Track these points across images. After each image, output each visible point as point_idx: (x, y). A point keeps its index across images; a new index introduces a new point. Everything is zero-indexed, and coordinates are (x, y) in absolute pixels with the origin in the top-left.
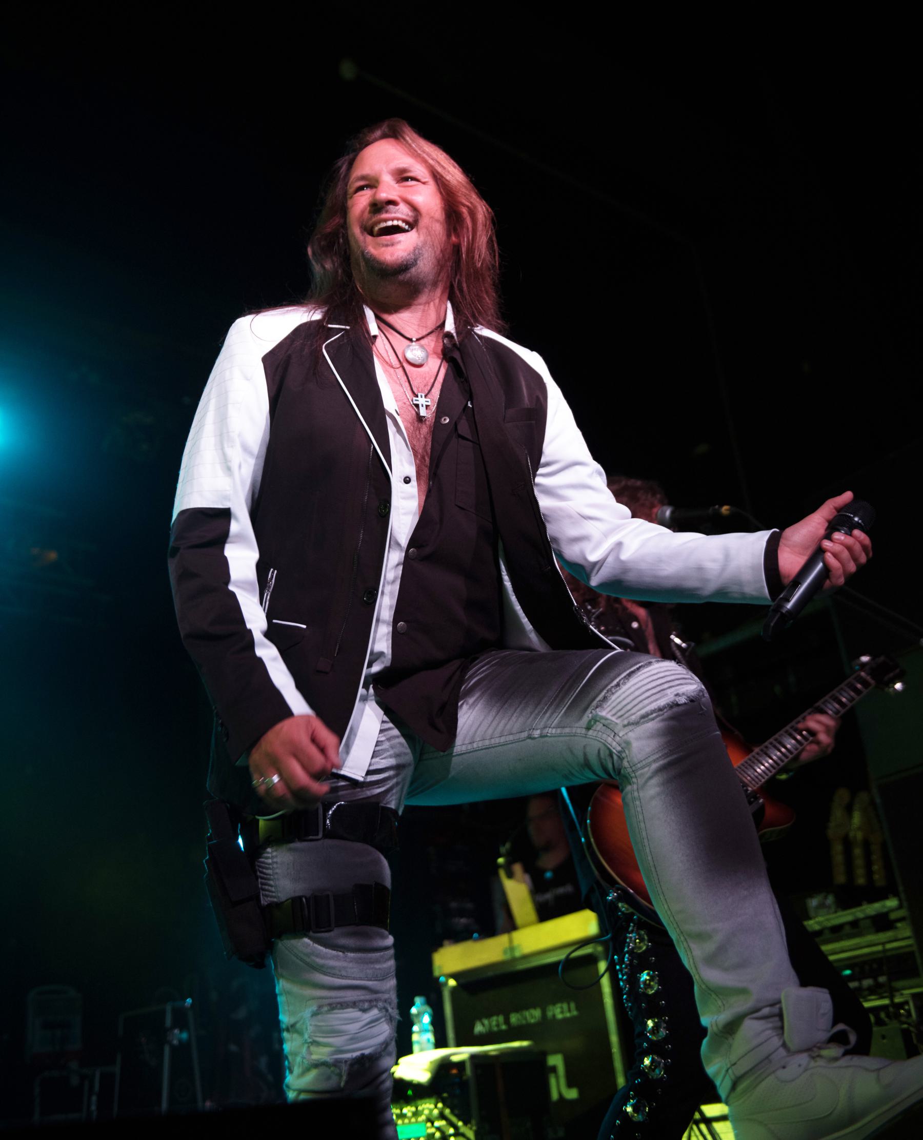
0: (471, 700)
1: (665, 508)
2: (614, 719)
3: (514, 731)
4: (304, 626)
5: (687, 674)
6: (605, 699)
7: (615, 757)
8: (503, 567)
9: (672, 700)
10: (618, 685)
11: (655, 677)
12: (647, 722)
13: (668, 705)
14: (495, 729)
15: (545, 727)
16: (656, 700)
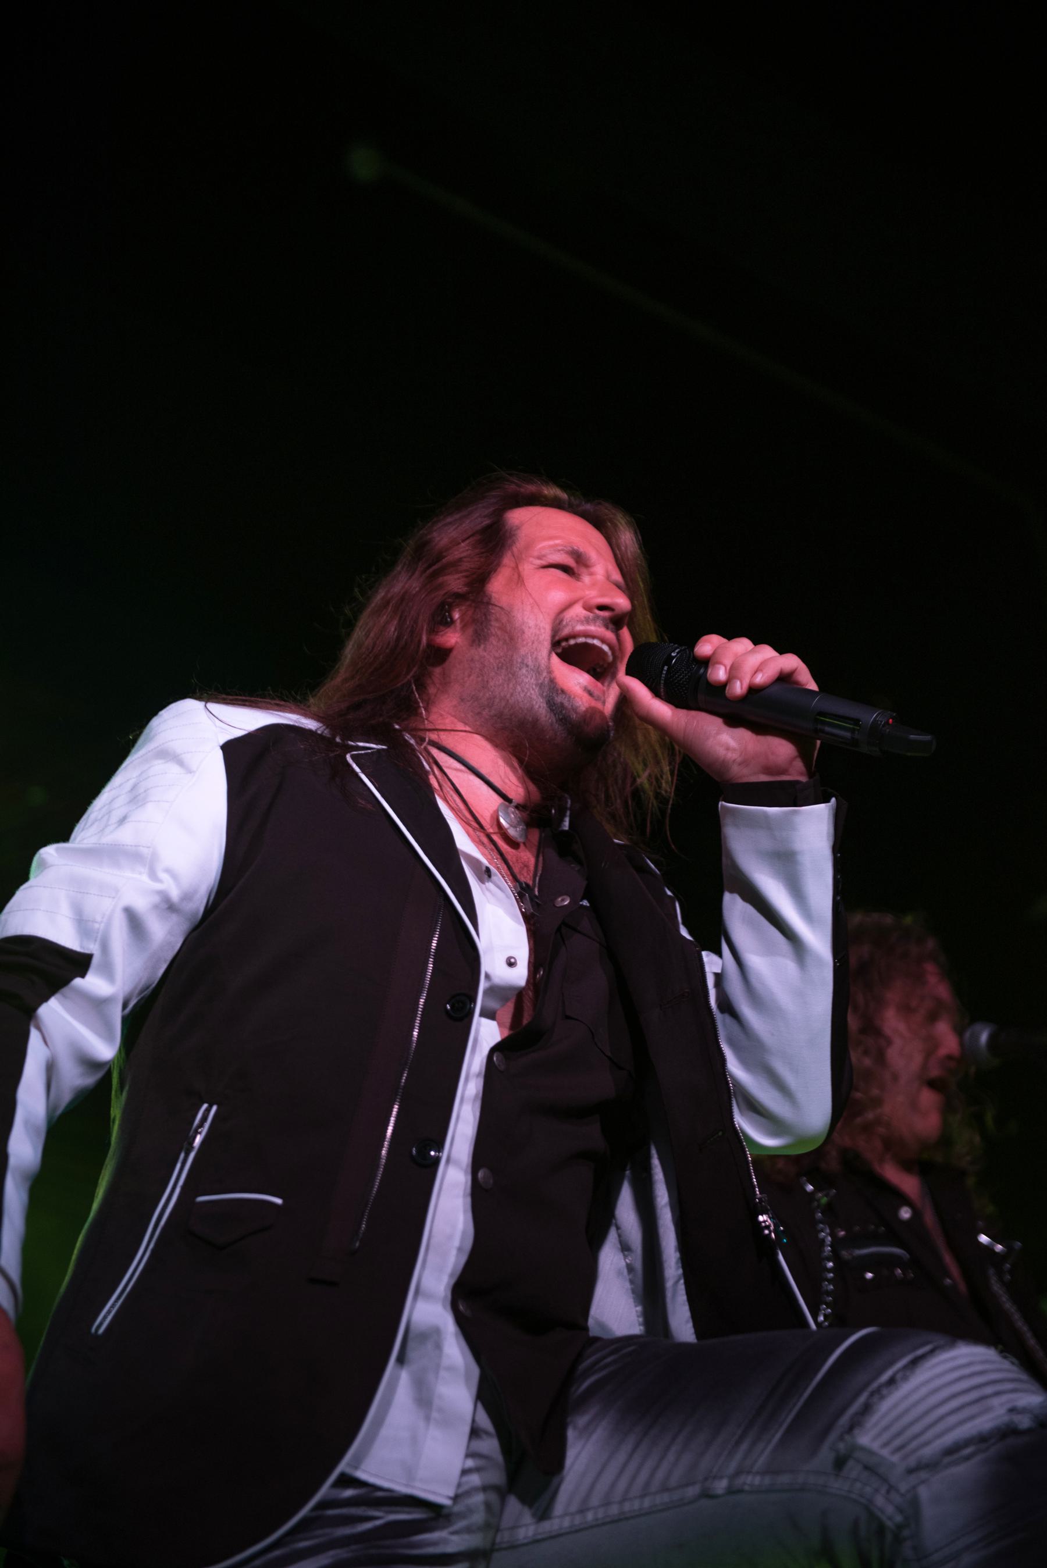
0: (582, 1420)
1: (977, 1027)
2: (885, 1452)
3: (673, 1482)
4: (278, 1201)
6: (867, 1409)
7: (889, 1537)
8: (656, 1162)
12: (955, 1463)
14: (634, 1478)
15: (738, 1473)
16: (972, 1417)
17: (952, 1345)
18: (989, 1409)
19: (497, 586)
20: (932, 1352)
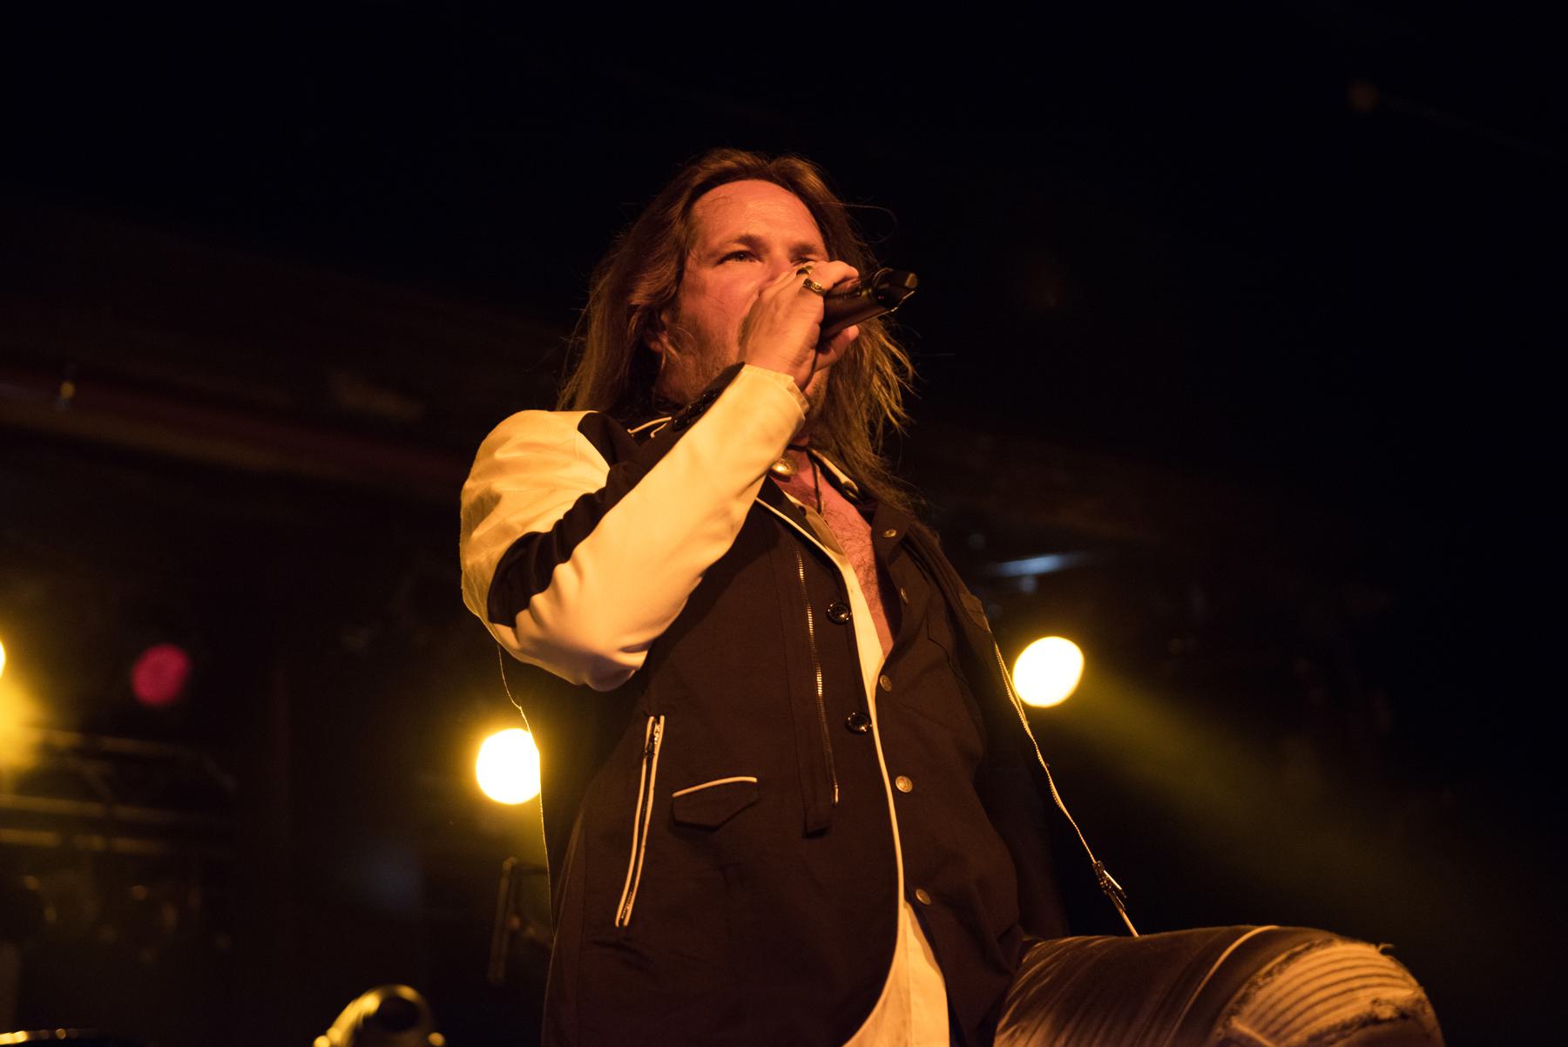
4: (754, 780)
5: (1404, 979)
9: (1368, 1009)
10: (1270, 973)
11: (1337, 966)
13: (1360, 1018)
16: (1337, 1007)
17: (1329, 943)
18: (1356, 999)
19: (807, 406)
20: (1308, 949)
